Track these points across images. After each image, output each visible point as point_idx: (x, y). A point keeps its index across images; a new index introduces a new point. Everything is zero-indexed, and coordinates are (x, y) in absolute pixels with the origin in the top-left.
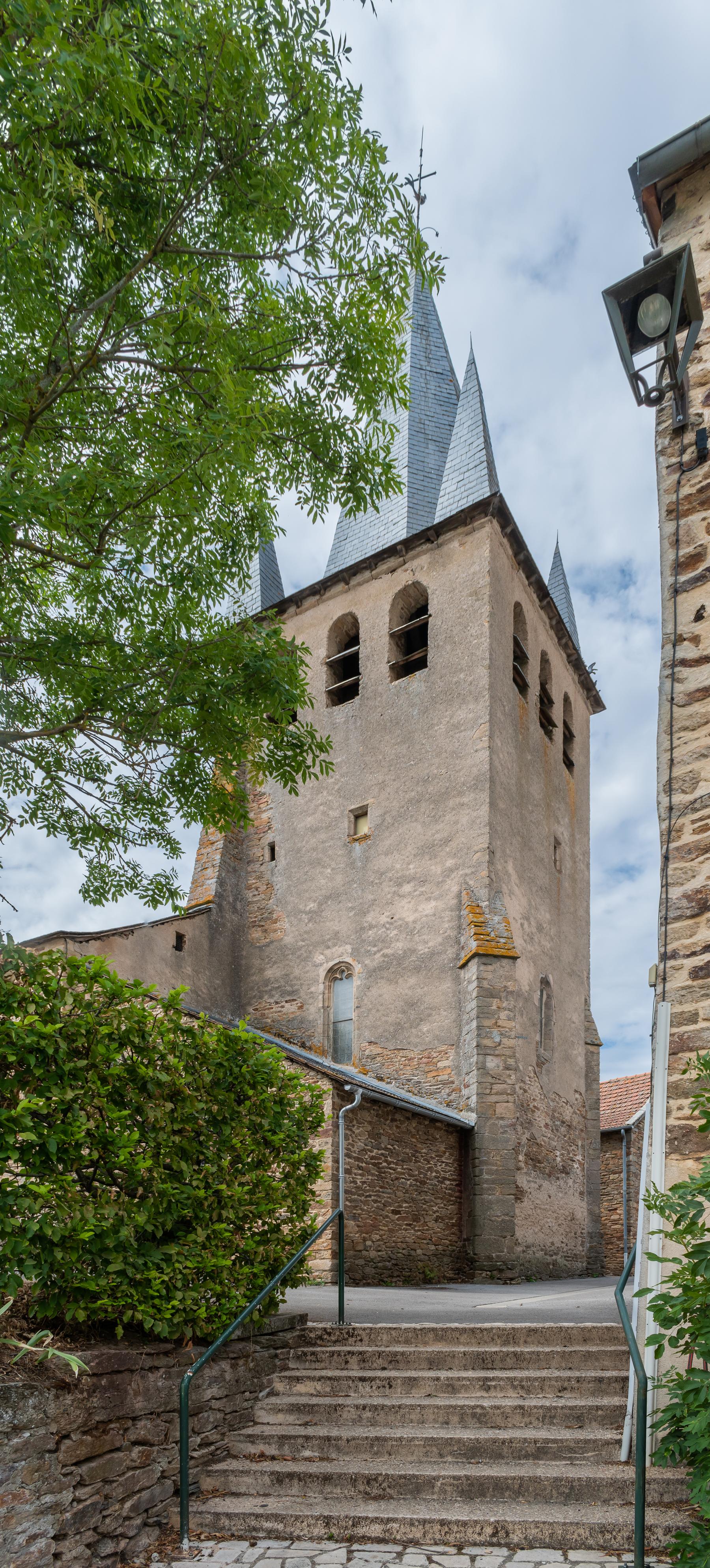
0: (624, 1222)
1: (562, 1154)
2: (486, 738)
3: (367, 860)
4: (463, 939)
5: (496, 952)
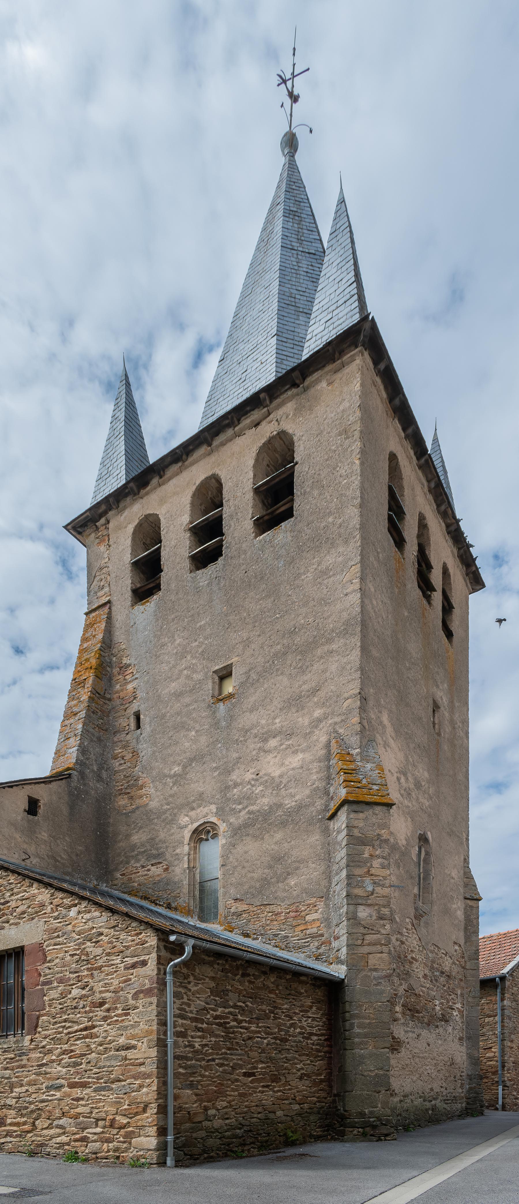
0: (498, 1059)
1: (442, 1003)
2: (358, 580)
3: (231, 718)
4: (332, 790)
5: (368, 798)
